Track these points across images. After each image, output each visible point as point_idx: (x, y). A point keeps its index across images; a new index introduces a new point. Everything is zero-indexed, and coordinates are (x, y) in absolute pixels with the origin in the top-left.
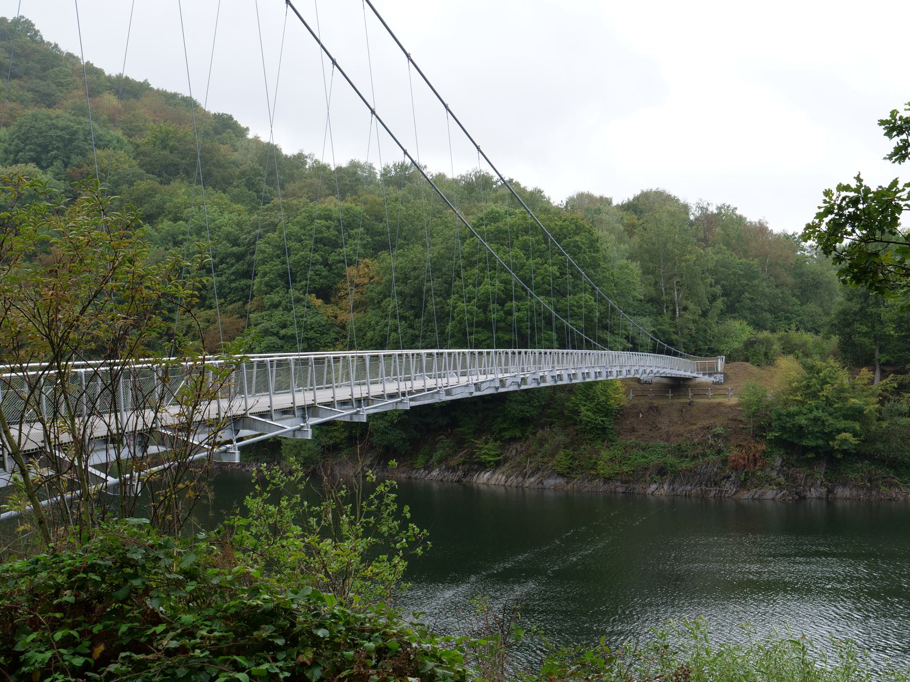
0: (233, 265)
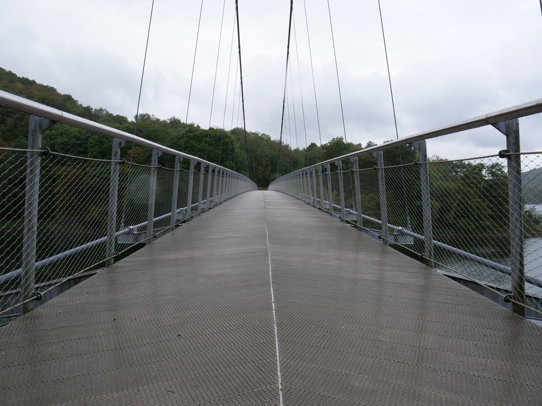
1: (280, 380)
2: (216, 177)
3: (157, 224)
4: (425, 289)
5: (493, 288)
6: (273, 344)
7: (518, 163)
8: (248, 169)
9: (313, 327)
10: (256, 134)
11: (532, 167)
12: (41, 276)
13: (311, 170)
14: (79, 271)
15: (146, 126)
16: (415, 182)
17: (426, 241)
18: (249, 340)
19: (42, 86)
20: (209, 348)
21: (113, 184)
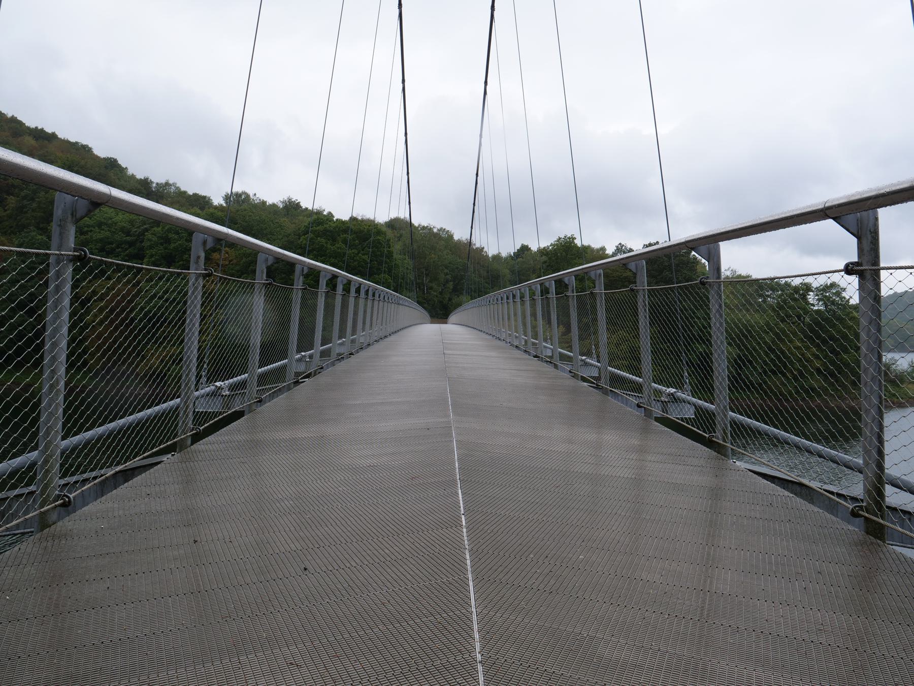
0: (126, 249)
1: (478, 646)
2: (361, 302)
3: (263, 379)
4: (716, 494)
5: (832, 493)
6: (464, 585)
7: (877, 284)
8: (414, 288)
9: (532, 556)
10: (428, 230)
11: (900, 289)
12: (71, 466)
13: (523, 290)
14: (134, 458)
15: (241, 211)
16: (694, 313)
17: (719, 414)
18: (425, 578)
19: (68, 142)
20: (357, 590)
21: (192, 311)
